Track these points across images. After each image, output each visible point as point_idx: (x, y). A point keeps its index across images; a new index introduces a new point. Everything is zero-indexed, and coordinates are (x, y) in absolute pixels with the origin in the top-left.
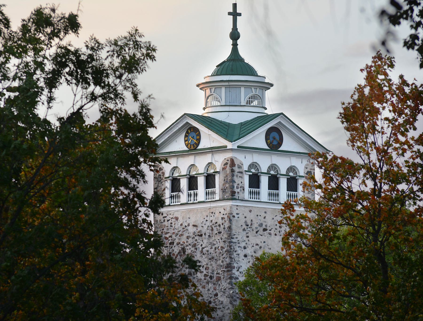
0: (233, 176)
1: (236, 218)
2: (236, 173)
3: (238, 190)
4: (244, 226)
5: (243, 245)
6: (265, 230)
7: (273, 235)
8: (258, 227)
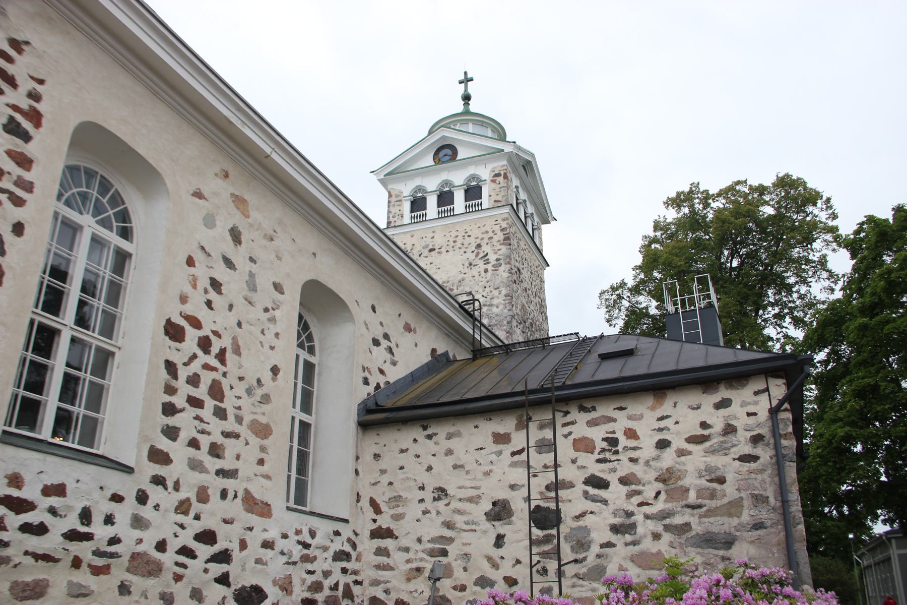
6: (431, 250)
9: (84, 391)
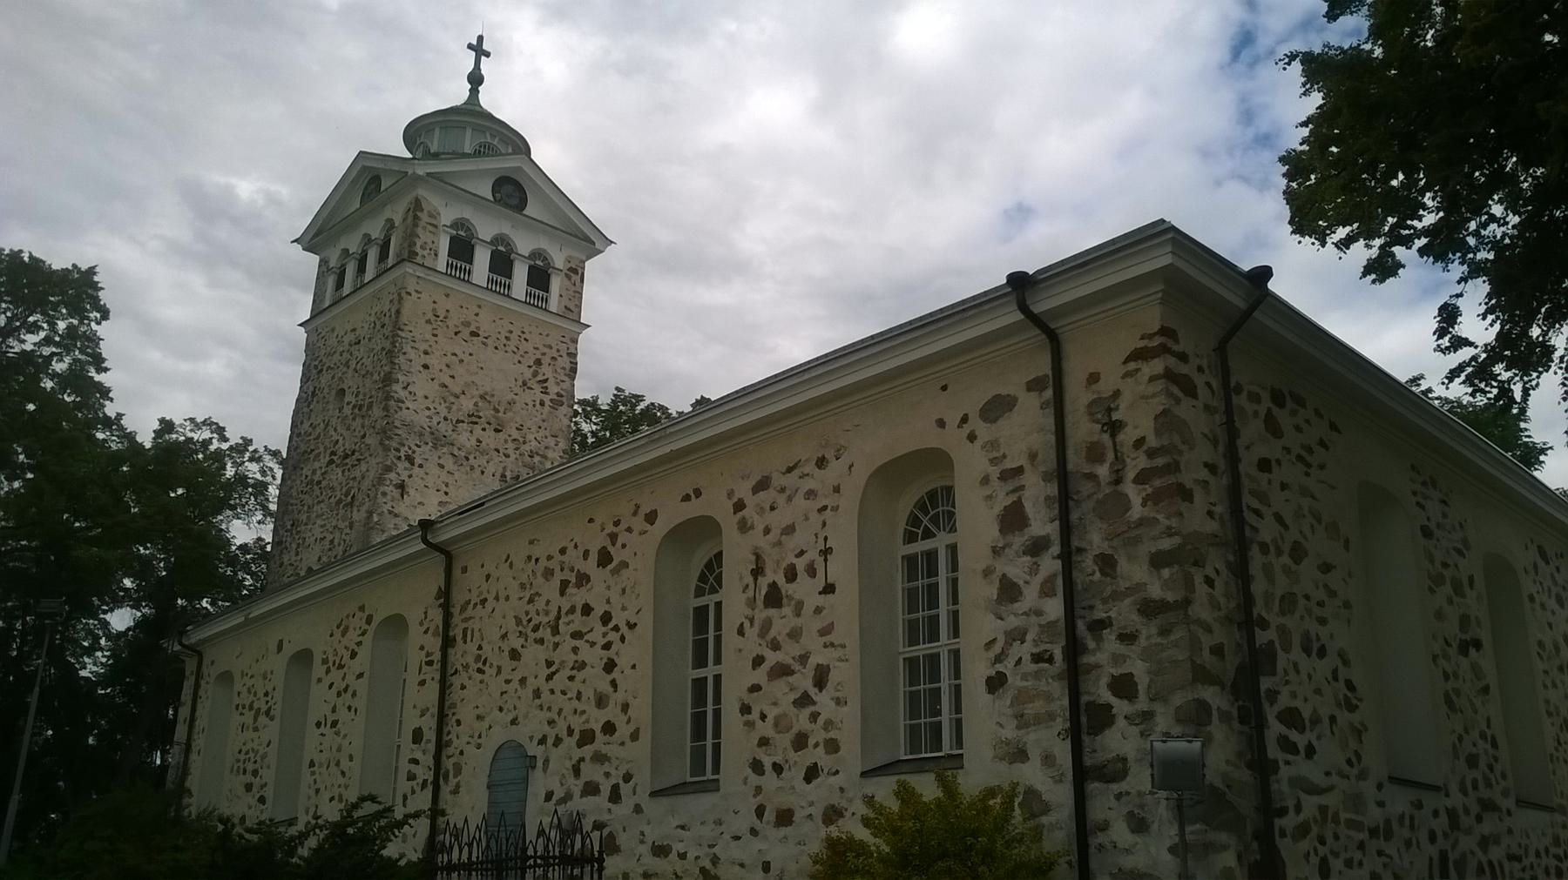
0: (415, 225)
2: (422, 224)
3: (425, 253)
4: (430, 316)
5: (424, 346)
6: (474, 334)
7: (491, 348)
8: (794, 730)
9: (922, 599)
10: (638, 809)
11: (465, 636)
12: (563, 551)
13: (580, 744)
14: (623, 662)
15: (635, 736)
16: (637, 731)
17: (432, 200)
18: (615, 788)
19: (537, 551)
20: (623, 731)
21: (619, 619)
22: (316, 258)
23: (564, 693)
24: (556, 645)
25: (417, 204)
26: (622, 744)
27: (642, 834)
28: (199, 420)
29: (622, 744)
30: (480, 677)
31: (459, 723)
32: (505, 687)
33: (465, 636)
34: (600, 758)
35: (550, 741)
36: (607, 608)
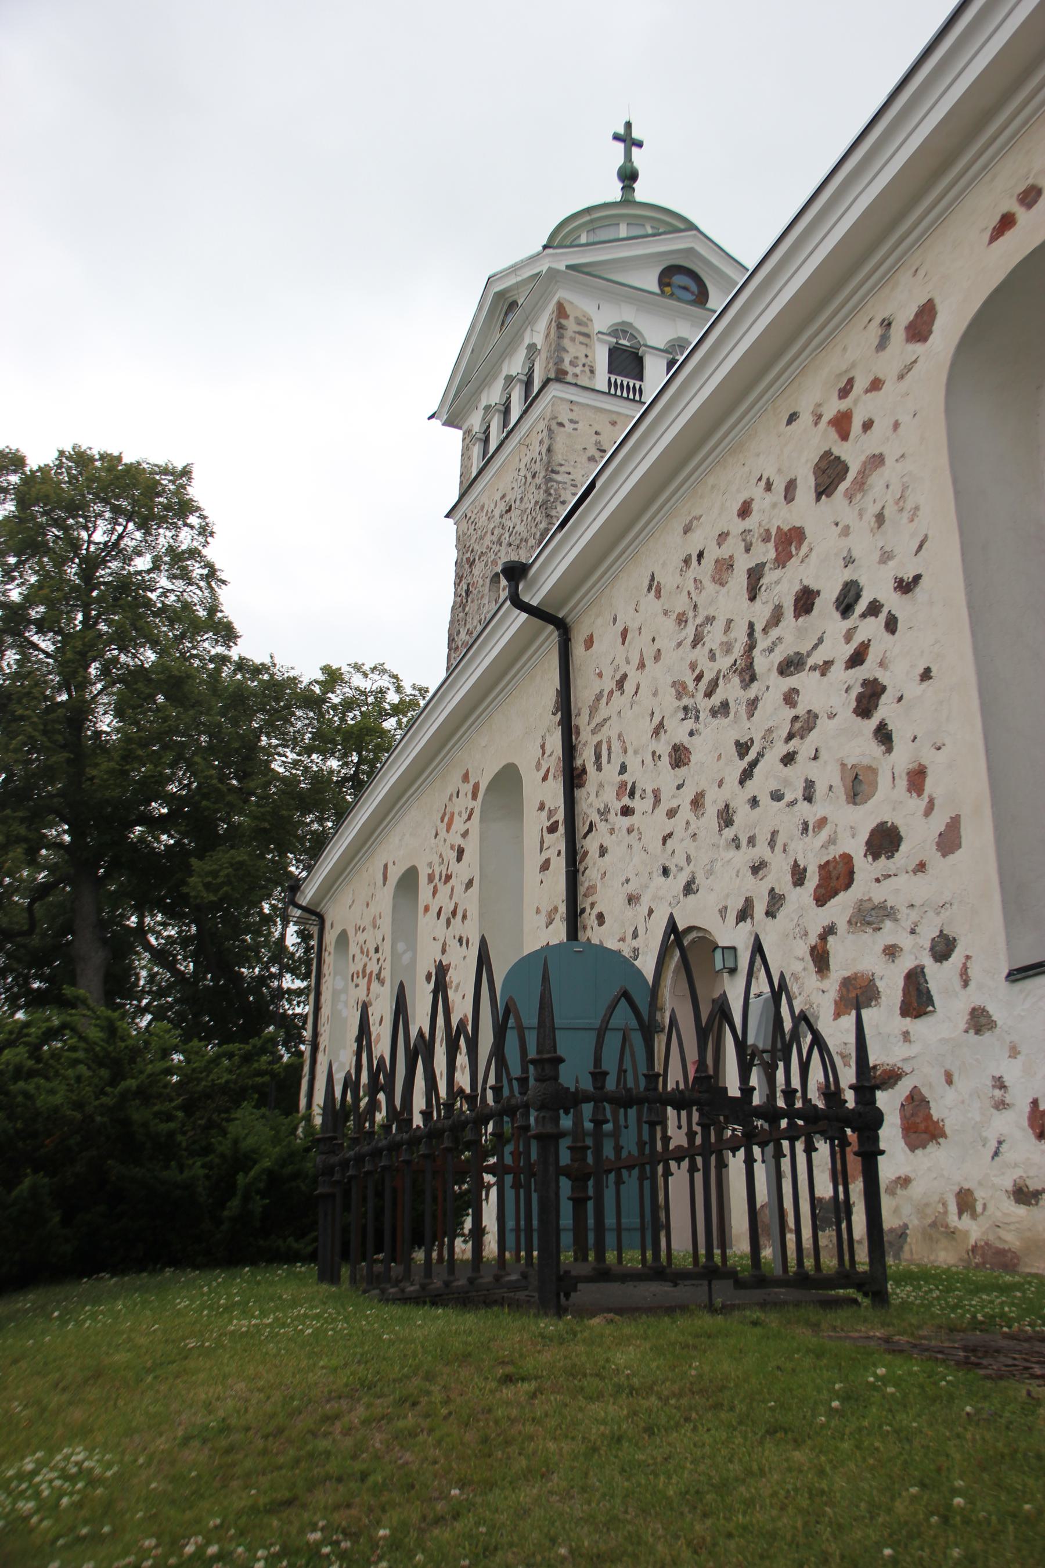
0: (561, 337)
1: (569, 427)
2: (569, 333)
3: (578, 370)
4: (592, 451)
10: (980, 1021)
11: (598, 756)
12: (745, 511)
13: (821, 899)
14: (898, 678)
15: (949, 841)
16: (954, 825)
17: (581, 303)
18: (915, 980)
19: (702, 538)
20: (919, 835)
21: (877, 586)
22: (458, 434)
23: (777, 796)
24: (753, 704)
25: (561, 311)
26: (921, 867)
27: (1000, 1084)
28: (366, 668)
29: (921, 867)
30: (626, 821)
31: (601, 918)
32: (669, 825)
33: (598, 756)
34: (871, 916)
35: (760, 908)
36: (847, 575)
